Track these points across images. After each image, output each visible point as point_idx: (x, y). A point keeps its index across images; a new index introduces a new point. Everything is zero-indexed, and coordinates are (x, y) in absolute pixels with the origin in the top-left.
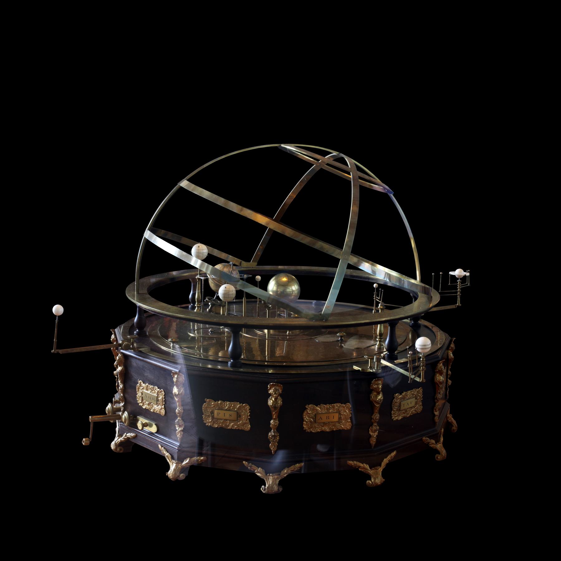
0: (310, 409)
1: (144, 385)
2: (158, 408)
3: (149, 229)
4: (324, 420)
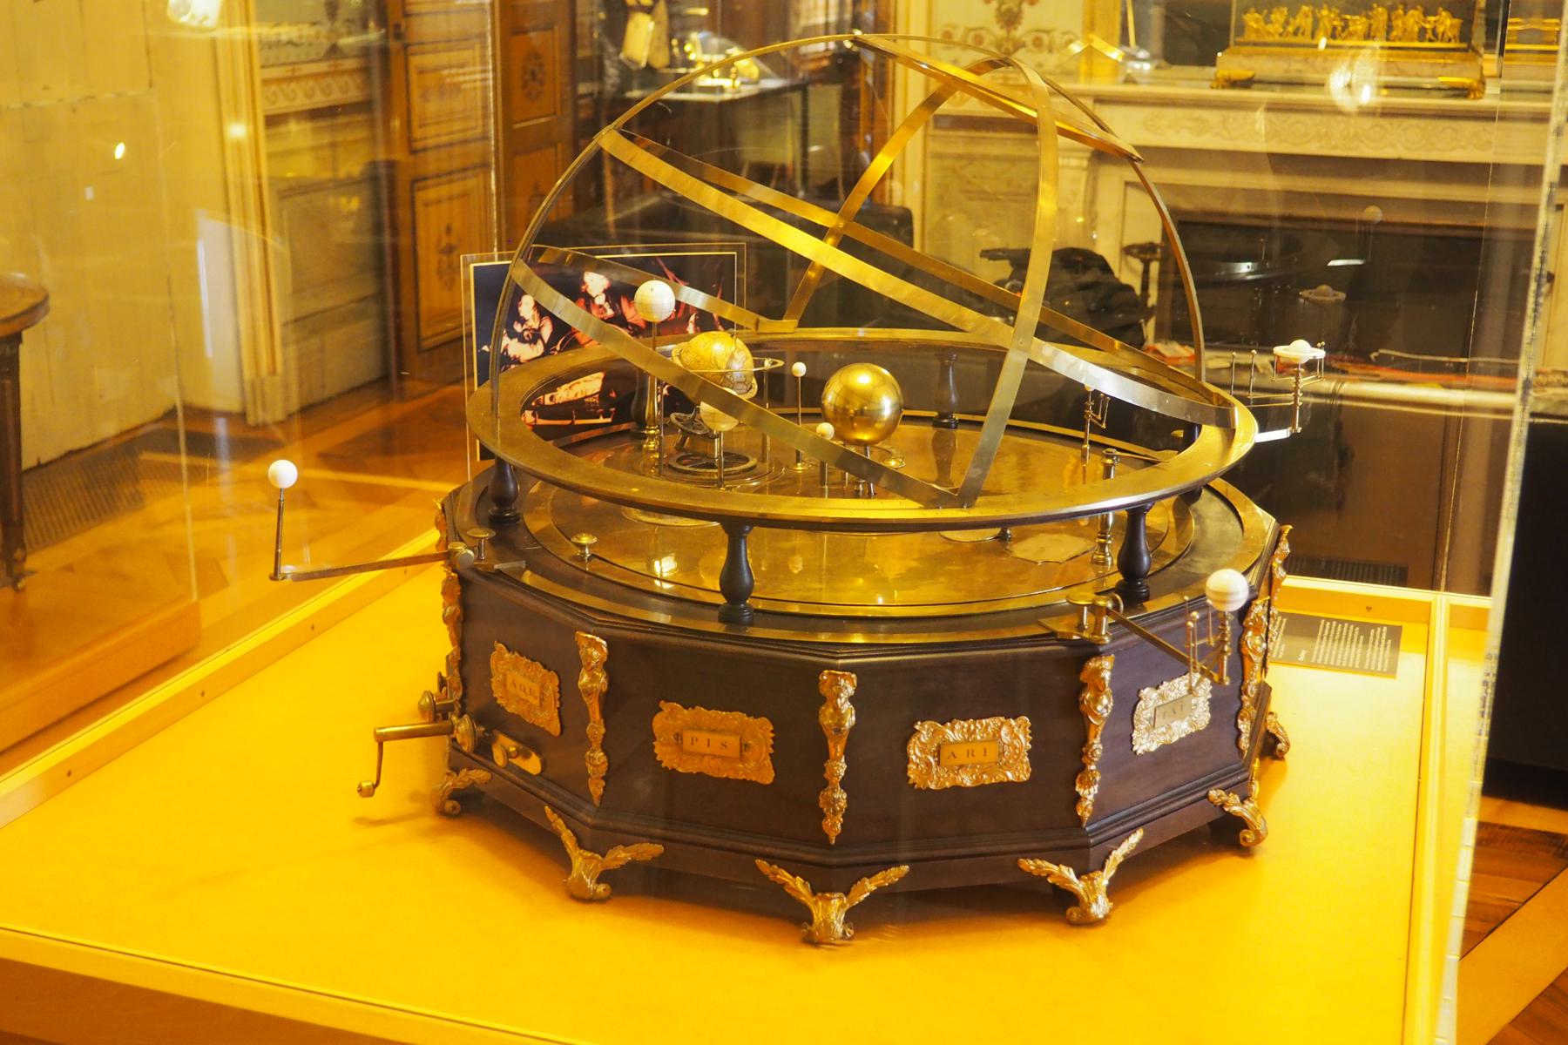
0: (925, 731)
1: (507, 655)
2: (548, 720)
3: (1207, 348)
4: (962, 757)
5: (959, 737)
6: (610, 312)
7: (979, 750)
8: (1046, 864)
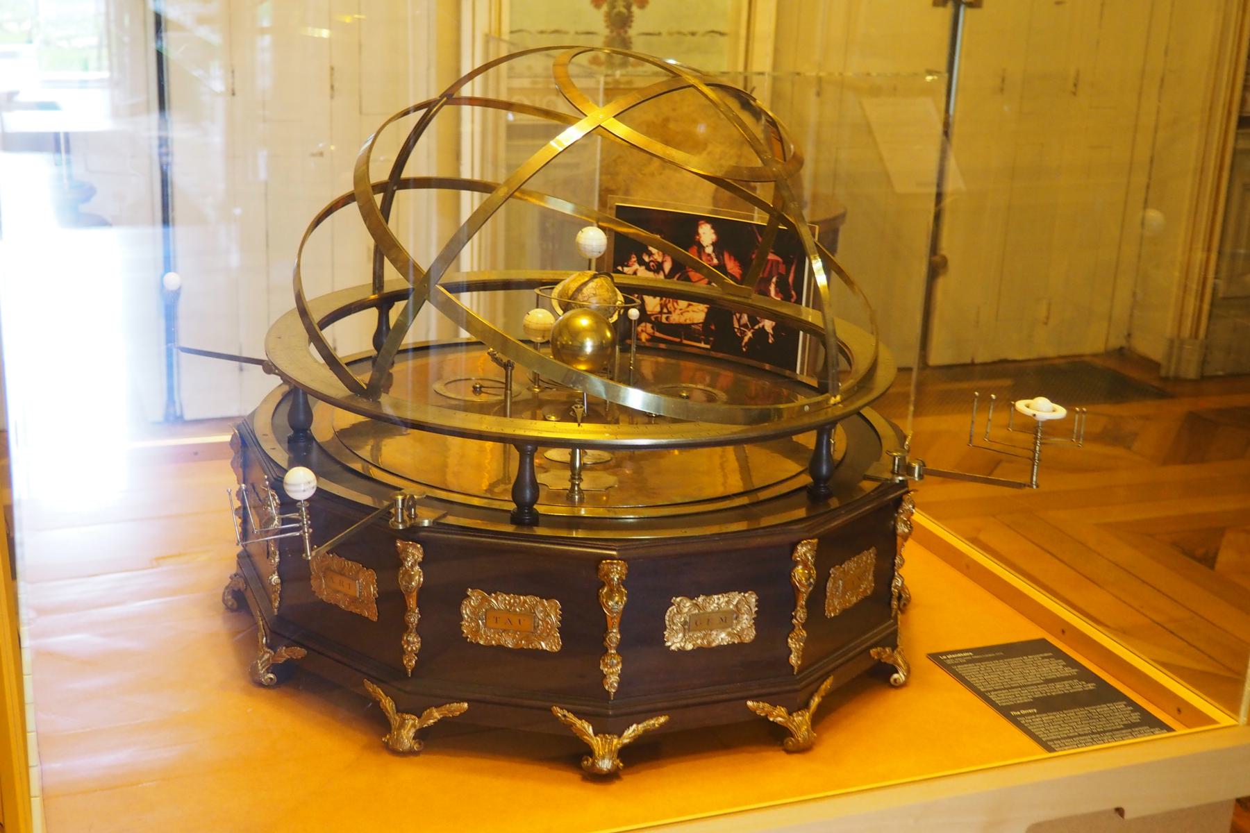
5: (502, 607)
6: (715, 261)
7: (515, 620)
8: (570, 716)
